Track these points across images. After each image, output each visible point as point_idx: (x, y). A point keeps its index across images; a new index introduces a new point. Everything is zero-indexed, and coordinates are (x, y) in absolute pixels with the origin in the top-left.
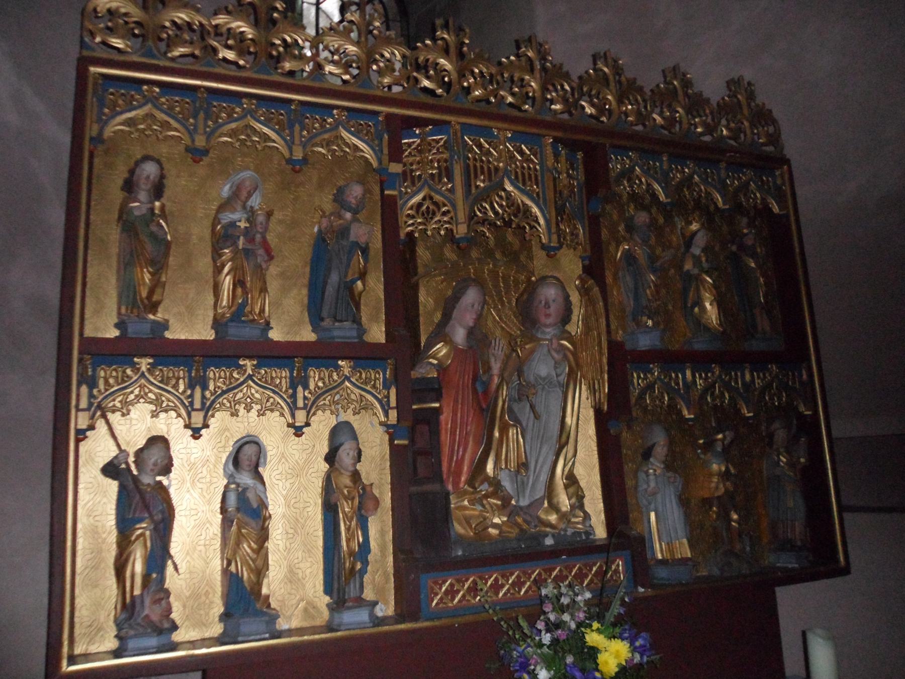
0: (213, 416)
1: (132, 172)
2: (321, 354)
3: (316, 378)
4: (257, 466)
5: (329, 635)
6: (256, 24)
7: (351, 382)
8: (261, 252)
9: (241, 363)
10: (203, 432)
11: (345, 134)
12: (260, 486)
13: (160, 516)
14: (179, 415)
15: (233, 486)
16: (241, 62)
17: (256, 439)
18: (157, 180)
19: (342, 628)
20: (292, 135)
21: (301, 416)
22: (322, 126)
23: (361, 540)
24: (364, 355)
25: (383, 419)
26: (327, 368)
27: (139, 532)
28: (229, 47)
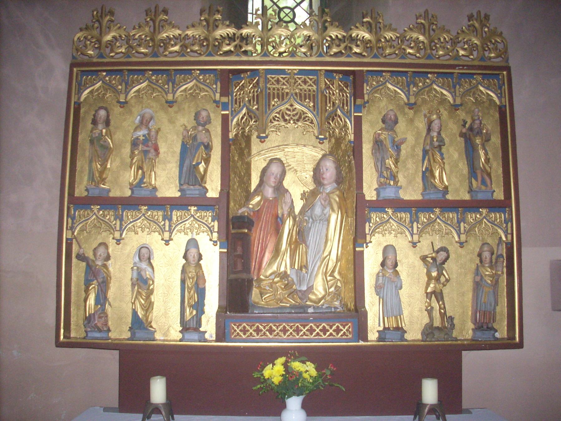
0: (374, 235)
1: (94, 116)
2: (472, 206)
3: (423, 218)
4: (149, 259)
5: (422, 343)
6: (370, 32)
7: (487, 219)
8: (152, 151)
9: (189, 208)
10: (170, 242)
11: (390, 86)
12: (150, 269)
13: (102, 280)
14: (208, 235)
15: (135, 268)
16: (364, 54)
17: (147, 246)
18: (106, 118)
19: (386, 340)
20: (455, 92)
21: (416, 238)
22: (424, 84)
23: (196, 300)
24: (205, 204)
25: (410, 240)
26: (427, 212)
27: (93, 286)
28: (412, 48)
